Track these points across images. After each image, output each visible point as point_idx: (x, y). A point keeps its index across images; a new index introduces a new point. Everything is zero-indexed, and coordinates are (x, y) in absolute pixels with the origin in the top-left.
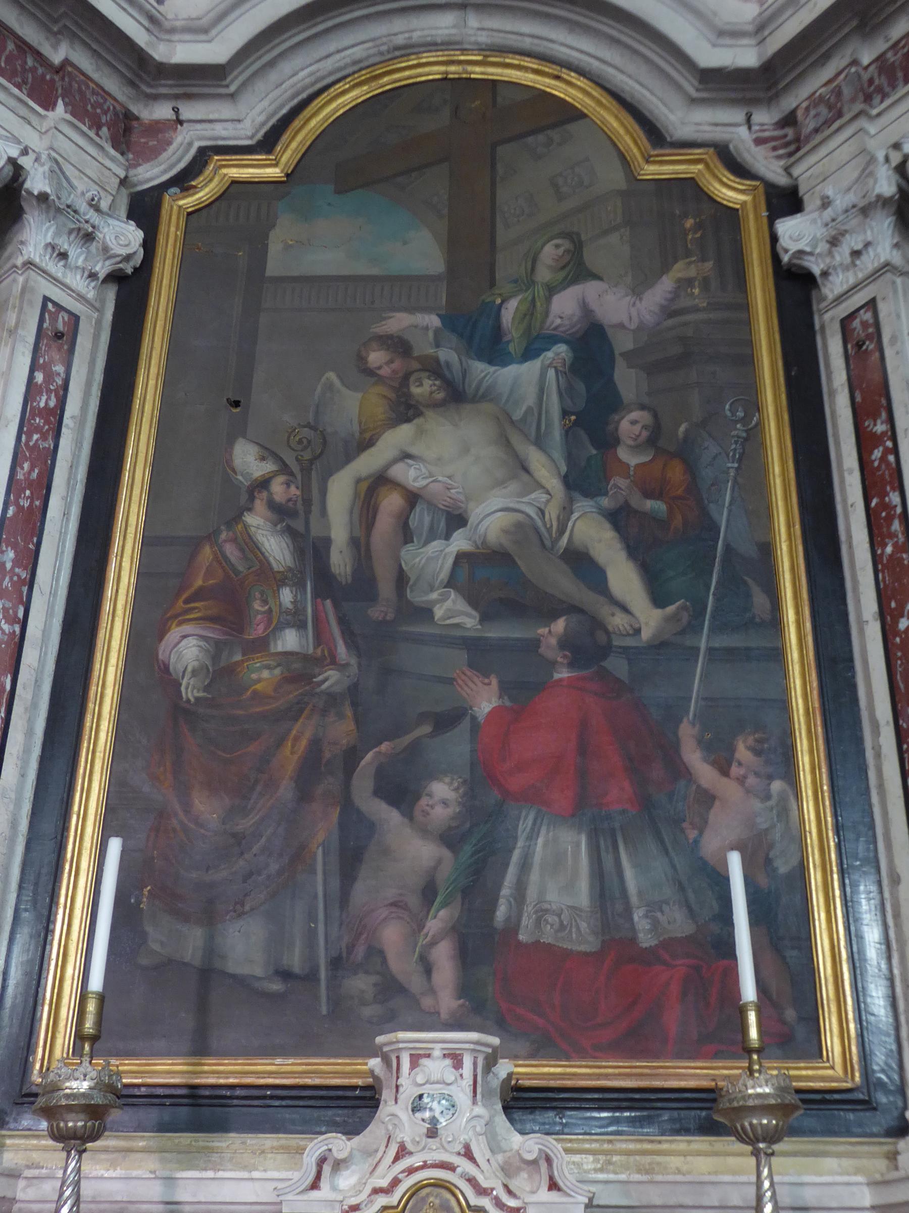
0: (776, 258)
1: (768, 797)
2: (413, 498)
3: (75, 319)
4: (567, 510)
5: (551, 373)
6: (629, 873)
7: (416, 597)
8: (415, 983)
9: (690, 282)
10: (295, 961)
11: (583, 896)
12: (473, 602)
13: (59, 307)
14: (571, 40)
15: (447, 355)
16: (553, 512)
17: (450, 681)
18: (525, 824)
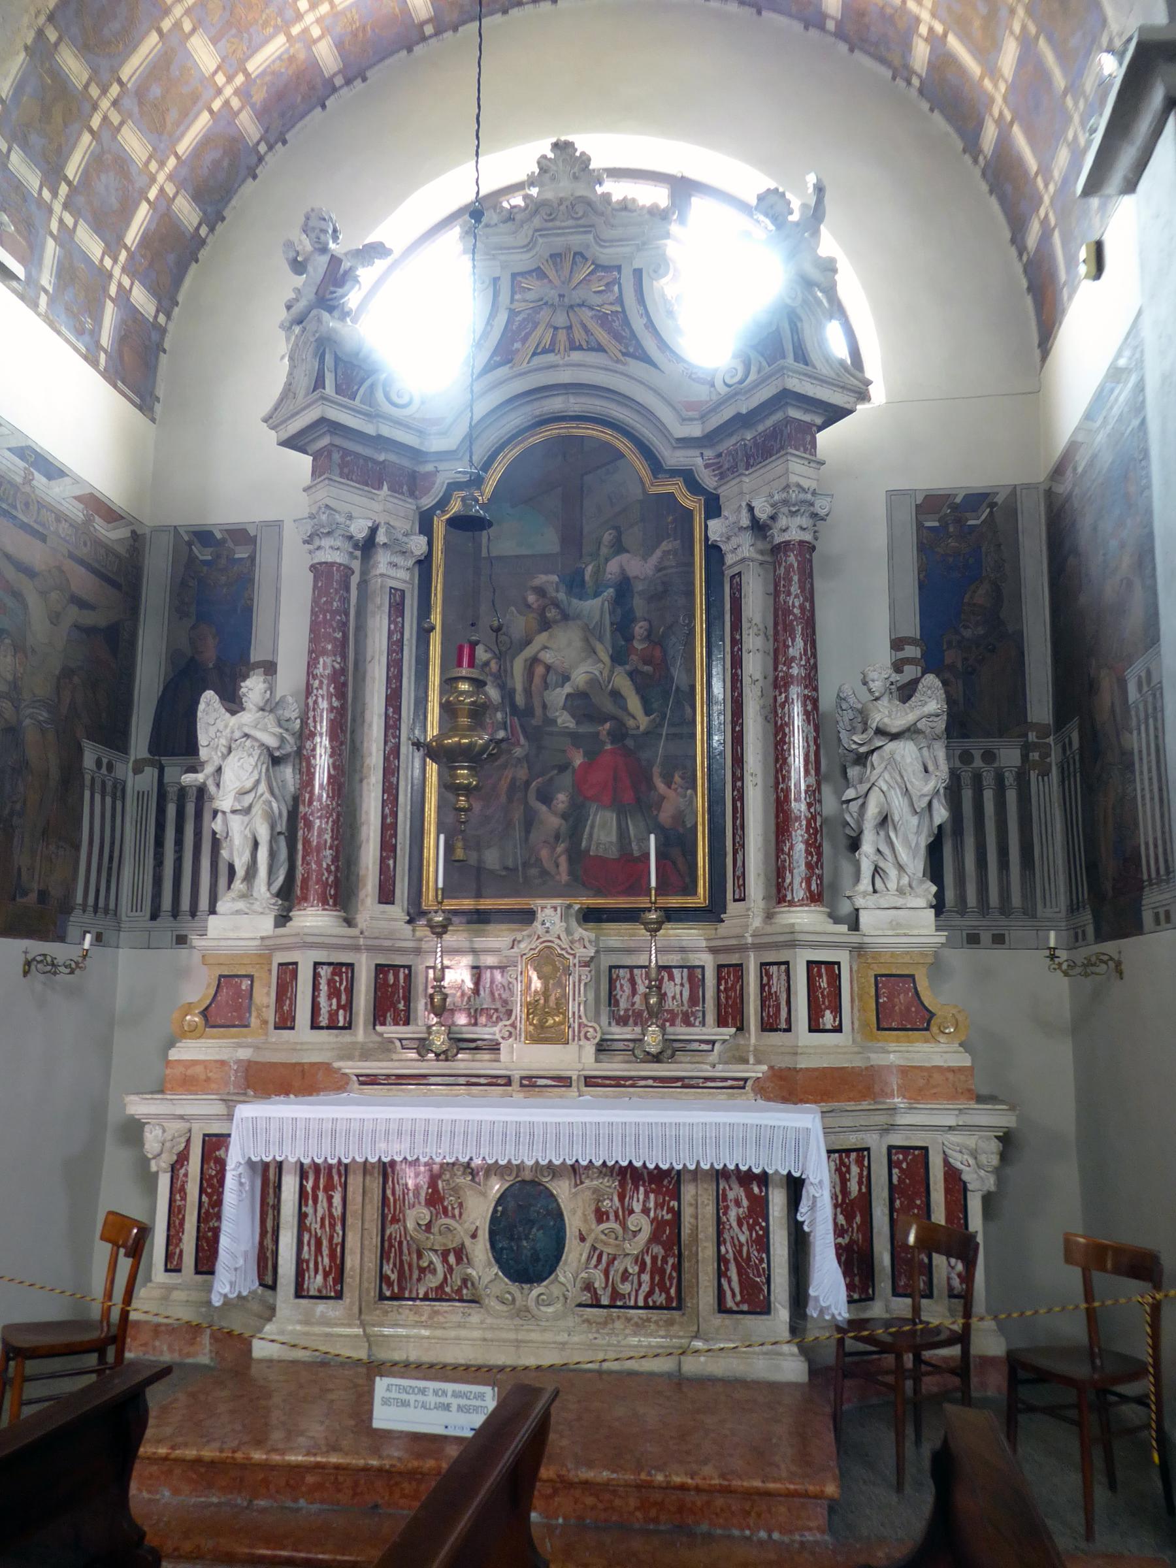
0: (707, 538)
1: (685, 796)
2: (548, 668)
3: (403, 592)
4: (612, 672)
5: (606, 603)
6: (631, 828)
7: (551, 714)
8: (553, 870)
9: (668, 552)
10: (510, 864)
11: (614, 838)
12: (573, 716)
13: (396, 589)
14: (619, 409)
15: (561, 596)
16: (606, 674)
17: (564, 751)
18: (593, 810)
